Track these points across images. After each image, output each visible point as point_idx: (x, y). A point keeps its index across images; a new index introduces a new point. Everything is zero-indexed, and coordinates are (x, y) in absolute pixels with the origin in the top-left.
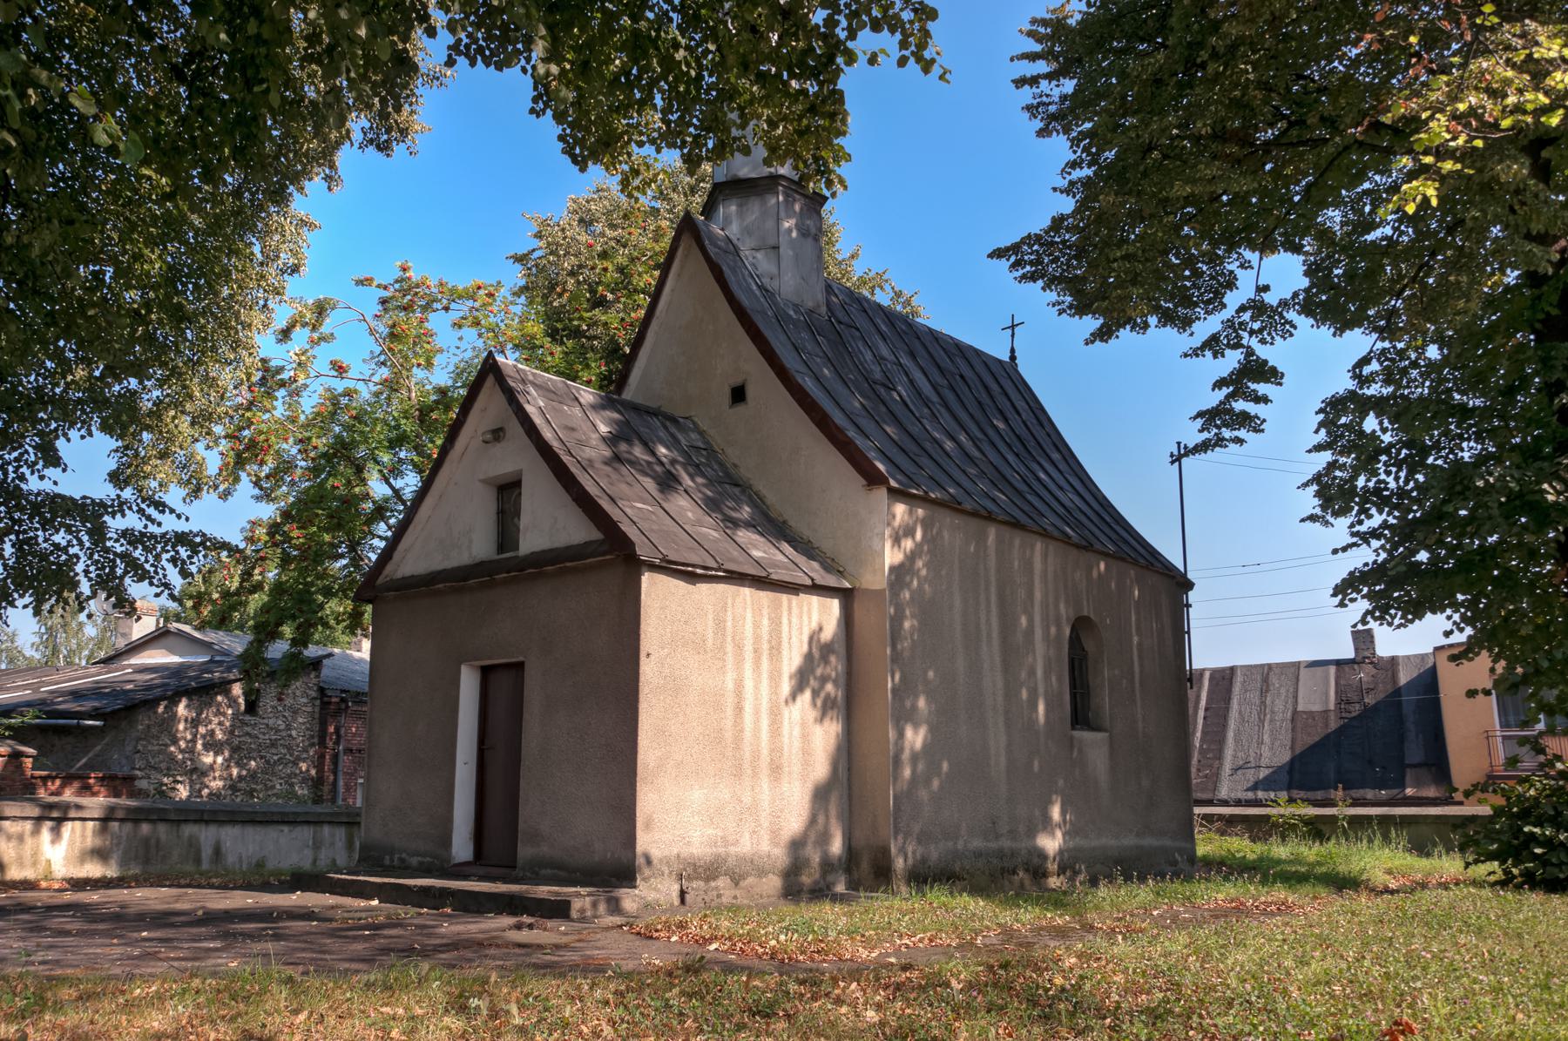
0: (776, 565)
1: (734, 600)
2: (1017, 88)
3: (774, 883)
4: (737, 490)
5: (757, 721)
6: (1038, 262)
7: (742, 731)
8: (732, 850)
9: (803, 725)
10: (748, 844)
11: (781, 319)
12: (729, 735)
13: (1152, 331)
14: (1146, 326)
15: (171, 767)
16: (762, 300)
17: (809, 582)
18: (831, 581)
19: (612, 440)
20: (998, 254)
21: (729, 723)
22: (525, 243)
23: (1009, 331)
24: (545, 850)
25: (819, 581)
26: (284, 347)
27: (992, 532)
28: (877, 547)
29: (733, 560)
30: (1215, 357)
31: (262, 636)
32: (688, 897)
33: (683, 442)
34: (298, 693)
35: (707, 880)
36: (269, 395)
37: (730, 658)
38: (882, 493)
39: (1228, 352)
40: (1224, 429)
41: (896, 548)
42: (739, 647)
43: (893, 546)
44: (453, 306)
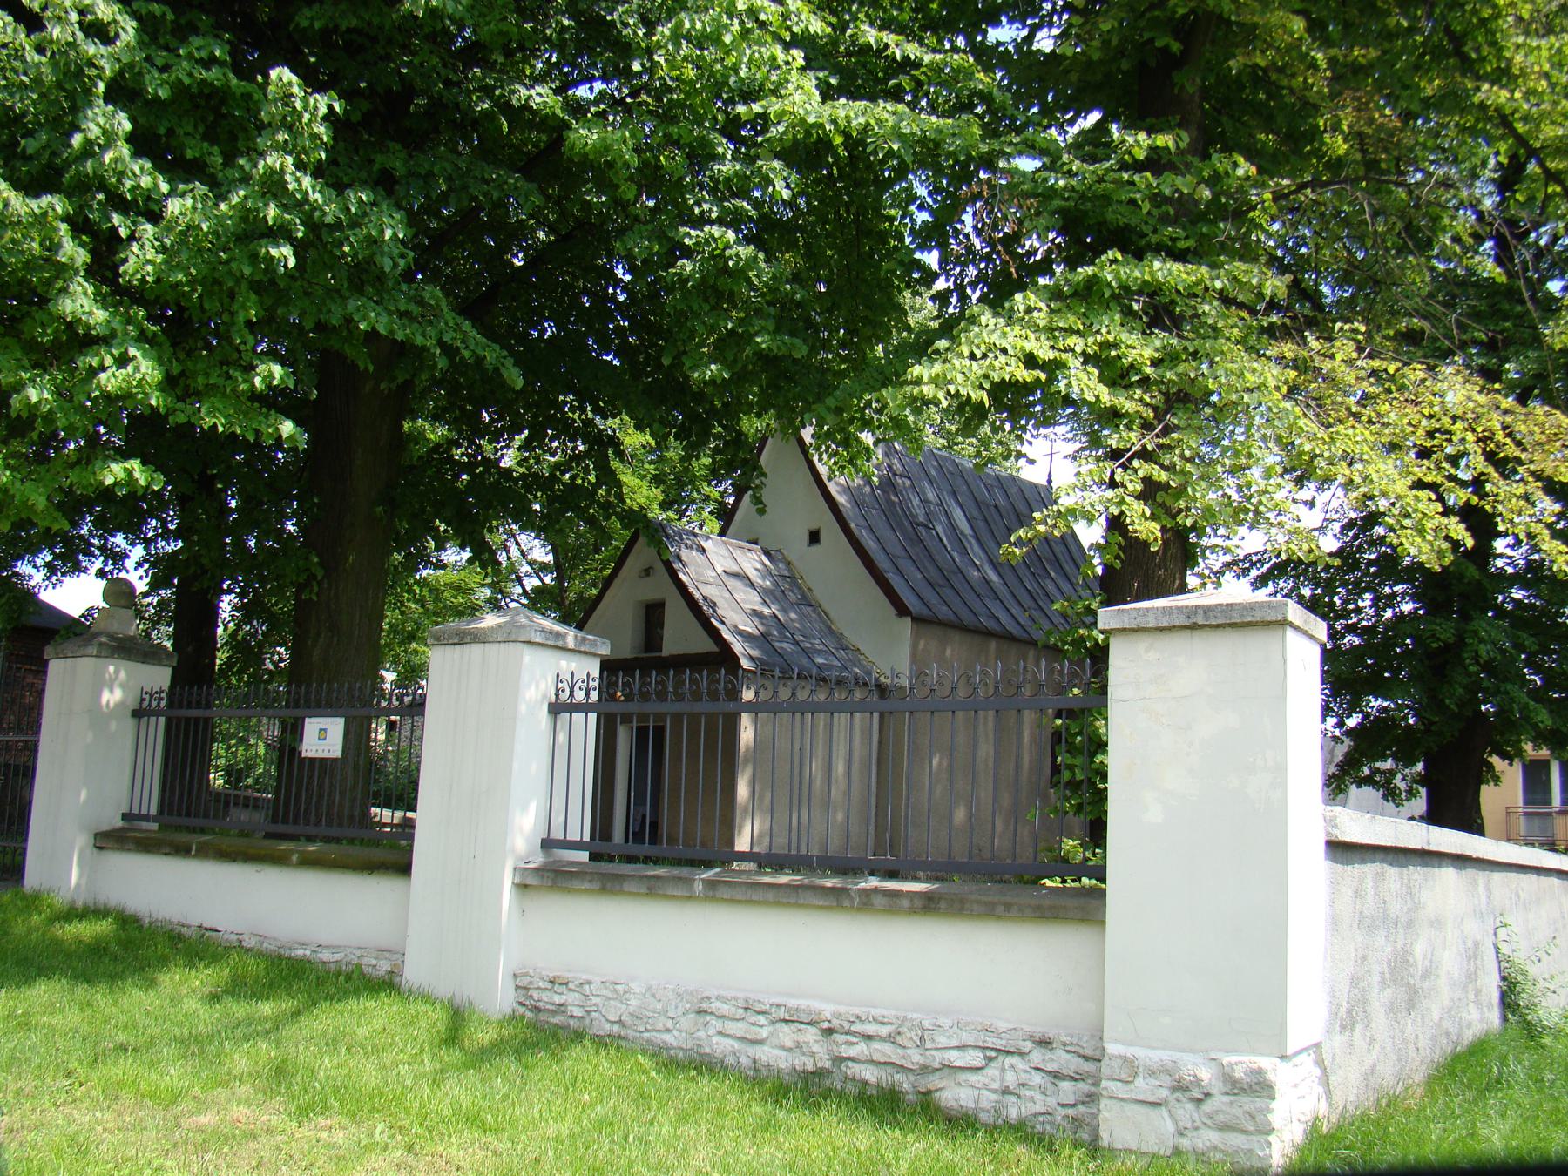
17: (997, 628)
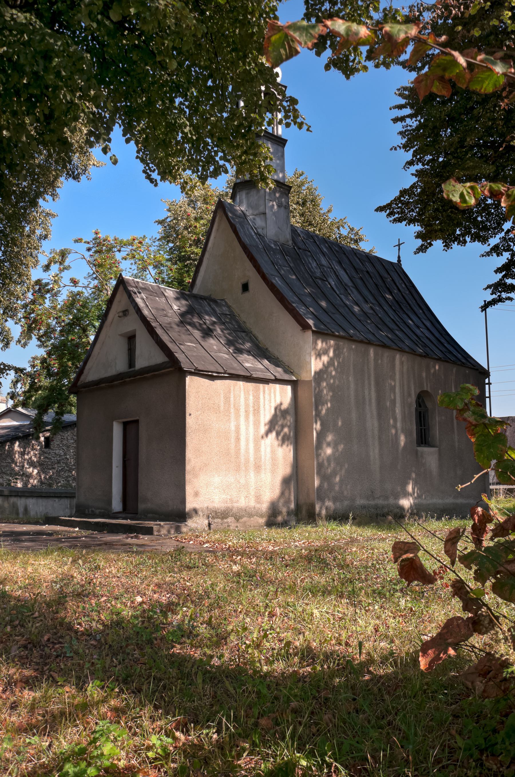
0: (256, 370)
1: (234, 387)
2: (394, 123)
3: (262, 521)
4: (243, 334)
5: (247, 444)
6: (402, 212)
7: (239, 449)
8: (235, 505)
9: (272, 446)
10: (244, 502)
11: (267, 248)
12: (233, 451)
13: (468, 244)
14: (465, 242)
15: (14, 474)
16: (257, 240)
17: (273, 378)
18: (286, 377)
19: (183, 315)
20: (380, 209)
21: (232, 446)
22: (164, 214)
23: (397, 247)
24: (149, 505)
25: (279, 377)
26: (47, 273)
27: (372, 352)
28: (308, 360)
29: (234, 369)
30: (498, 256)
31: (41, 411)
32: (212, 526)
33: (218, 312)
34: (69, 438)
35: (223, 518)
36: (43, 297)
37: (233, 415)
38: (309, 334)
39: (504, 253)
40: (503, 293)
41: (318, 359)
42: (237, 410)
43: (316, 359)
44: (122, 249)
